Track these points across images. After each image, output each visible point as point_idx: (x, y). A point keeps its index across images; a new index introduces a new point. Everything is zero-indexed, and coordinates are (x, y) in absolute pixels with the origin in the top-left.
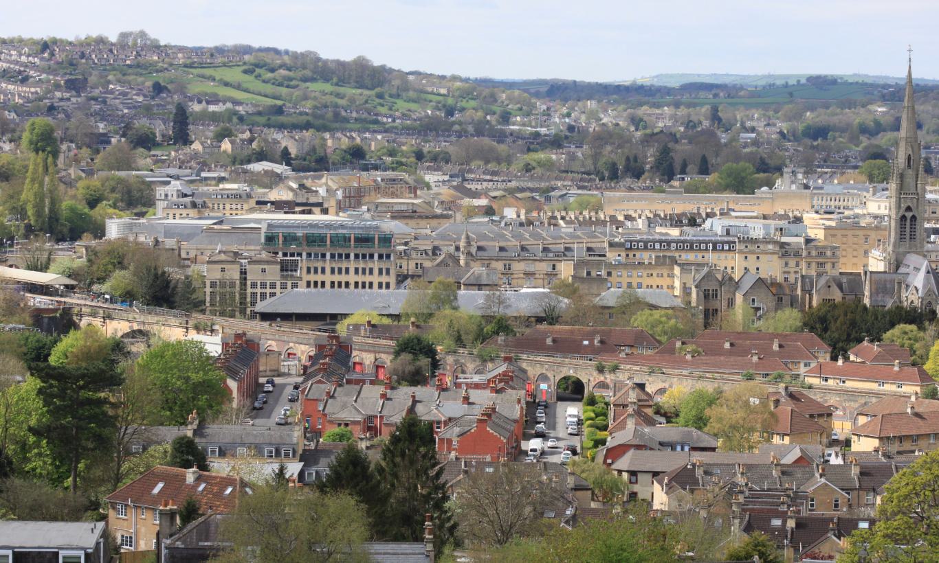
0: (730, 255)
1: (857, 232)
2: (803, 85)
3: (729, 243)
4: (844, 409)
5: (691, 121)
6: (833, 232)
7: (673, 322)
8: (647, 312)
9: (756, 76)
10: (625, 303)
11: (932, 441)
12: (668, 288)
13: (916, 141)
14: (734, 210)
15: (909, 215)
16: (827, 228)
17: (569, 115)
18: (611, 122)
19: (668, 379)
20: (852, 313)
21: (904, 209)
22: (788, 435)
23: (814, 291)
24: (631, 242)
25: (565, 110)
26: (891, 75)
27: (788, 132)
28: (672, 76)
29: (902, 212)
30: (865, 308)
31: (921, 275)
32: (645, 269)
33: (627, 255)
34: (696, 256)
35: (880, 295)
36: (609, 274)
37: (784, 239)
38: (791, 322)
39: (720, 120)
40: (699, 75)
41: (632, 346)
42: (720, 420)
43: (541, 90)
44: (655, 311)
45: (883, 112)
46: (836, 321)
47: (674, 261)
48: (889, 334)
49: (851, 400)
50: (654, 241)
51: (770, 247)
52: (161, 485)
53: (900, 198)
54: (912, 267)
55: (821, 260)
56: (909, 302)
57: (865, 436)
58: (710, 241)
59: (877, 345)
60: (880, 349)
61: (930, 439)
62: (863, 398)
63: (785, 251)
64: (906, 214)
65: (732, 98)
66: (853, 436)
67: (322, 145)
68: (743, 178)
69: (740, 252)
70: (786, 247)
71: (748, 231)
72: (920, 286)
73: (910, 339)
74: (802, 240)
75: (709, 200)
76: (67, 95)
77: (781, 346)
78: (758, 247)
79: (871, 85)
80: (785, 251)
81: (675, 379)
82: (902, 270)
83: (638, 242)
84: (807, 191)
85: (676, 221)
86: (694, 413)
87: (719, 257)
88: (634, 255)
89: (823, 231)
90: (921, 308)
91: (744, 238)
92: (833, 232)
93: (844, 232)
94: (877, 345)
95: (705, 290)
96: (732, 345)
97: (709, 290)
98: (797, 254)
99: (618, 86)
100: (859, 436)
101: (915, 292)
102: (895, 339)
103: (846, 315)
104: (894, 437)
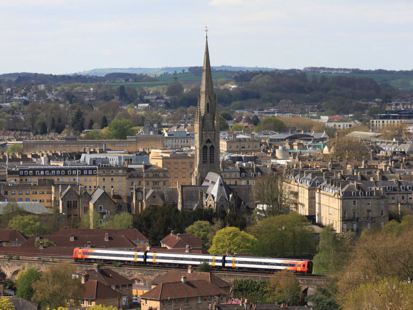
0: (93, 178)
1: (185, 161)
2: (186, 73)
3: (93, 169)
4: (144, 281)
5: (107, 97)
6: (168, 161)
7: (38, 224)
8: (19, 217)
9: (158, 69)
10: (9, 212)
11: (199, 302)
12: (48, 201)
13: (212, 94)
14: (110, 150)
15: (209, 145)
16: (164, 158)
17: (25, 95)
18: (54, 98)
19: (22, 263)
20: (167, 214)
21: (206, 141)
22: (94, 300)
23: (144, 201)
24: (24, 170)
25: (23, 91)
26: (250, 67)
27: (171, 102)
28: (103, 70)
30: (177, 210)
31: (216, 186)
32: (31, 189)
33: (22, 180)
34: (70, 179)
35: (188, 202)
36: (6, 193)
37: (130, 166)
38: (125, 222)
39: (126, 95)
40: (121, 69)
41: (8, 242)
42: (42, 291)
43: (12, 80)
44: (25, 217)
45: (234, 88)
46: (156, 221)
47: (52, 183)
48: (190, 228)
49: (149, 275)
50: (40, 170)
51: (121, 171)
53: (202, 134)
54: (210, 182)
55: (156, 180)
56: (208, 205)
57: (151, 300)
58: (79, 169)
59: (178, 236)
60: (180, 238)
61: (197, 300)
62: (158, 273)
63: (131, 174)
64: (207, 145)
65: (138, 82)
66: (142, 300)
67: (412, 213)
68: (125, 130)
69: (100, 175)
70: (132, 171)
71: (108, 161)
72: (215, 195)
73: (204, 231)
74: (142, 166)
75: (95, 144)
77: (110, 238)
78: (112, 172)
79: (231, 72)
80: (131, 174)
81: (27, 263)
82: (205, 184)
83: (29, 170)
84: (159, 135)
85: (63, 157)
86: (26, 287)
87: (86, 179)
88: (26, 180)
89: (161, 161)
90: (216, 209)
91: (102, 166)
92: (168, 161)
93: (175, 161)
94: (178, 236)
95: (68, 202)
96: (75, 238)
97: (71, 202)
98: (139, 177)
100: (146, 300)
101: (212, 199)
102: (194, 231)
103: (163, 216)
104: (171, 300)
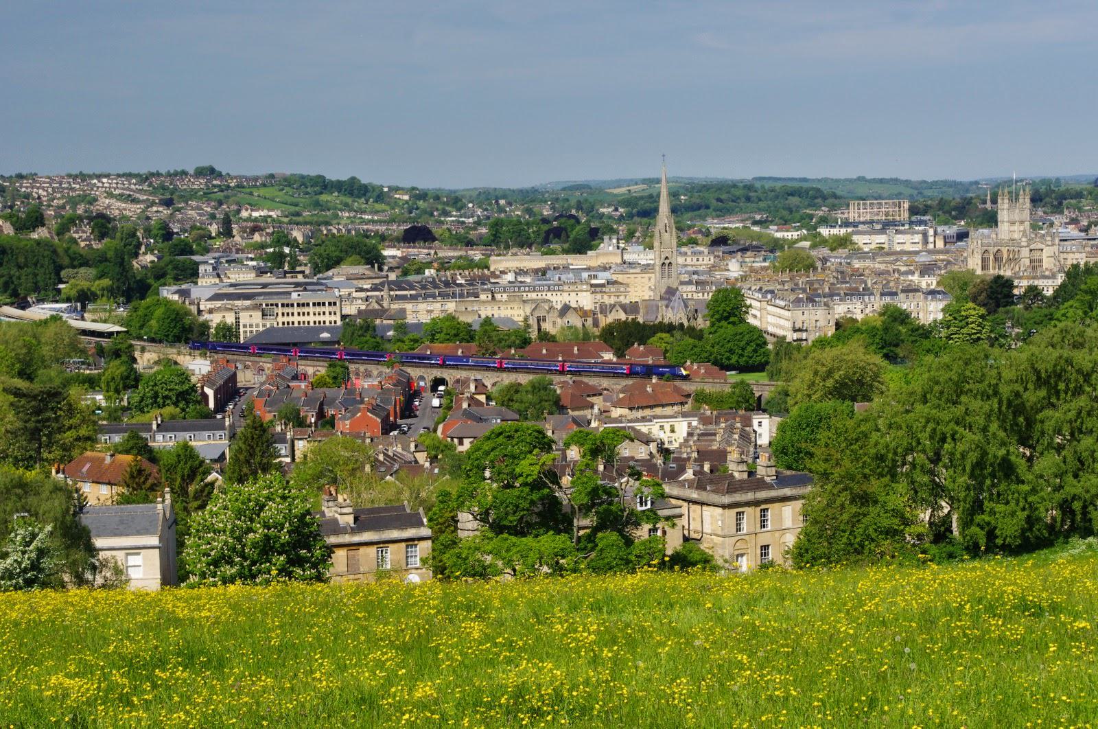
29: (663, 261)
52: (88, 466)
76: (161, 209)
99: (749, 187)
